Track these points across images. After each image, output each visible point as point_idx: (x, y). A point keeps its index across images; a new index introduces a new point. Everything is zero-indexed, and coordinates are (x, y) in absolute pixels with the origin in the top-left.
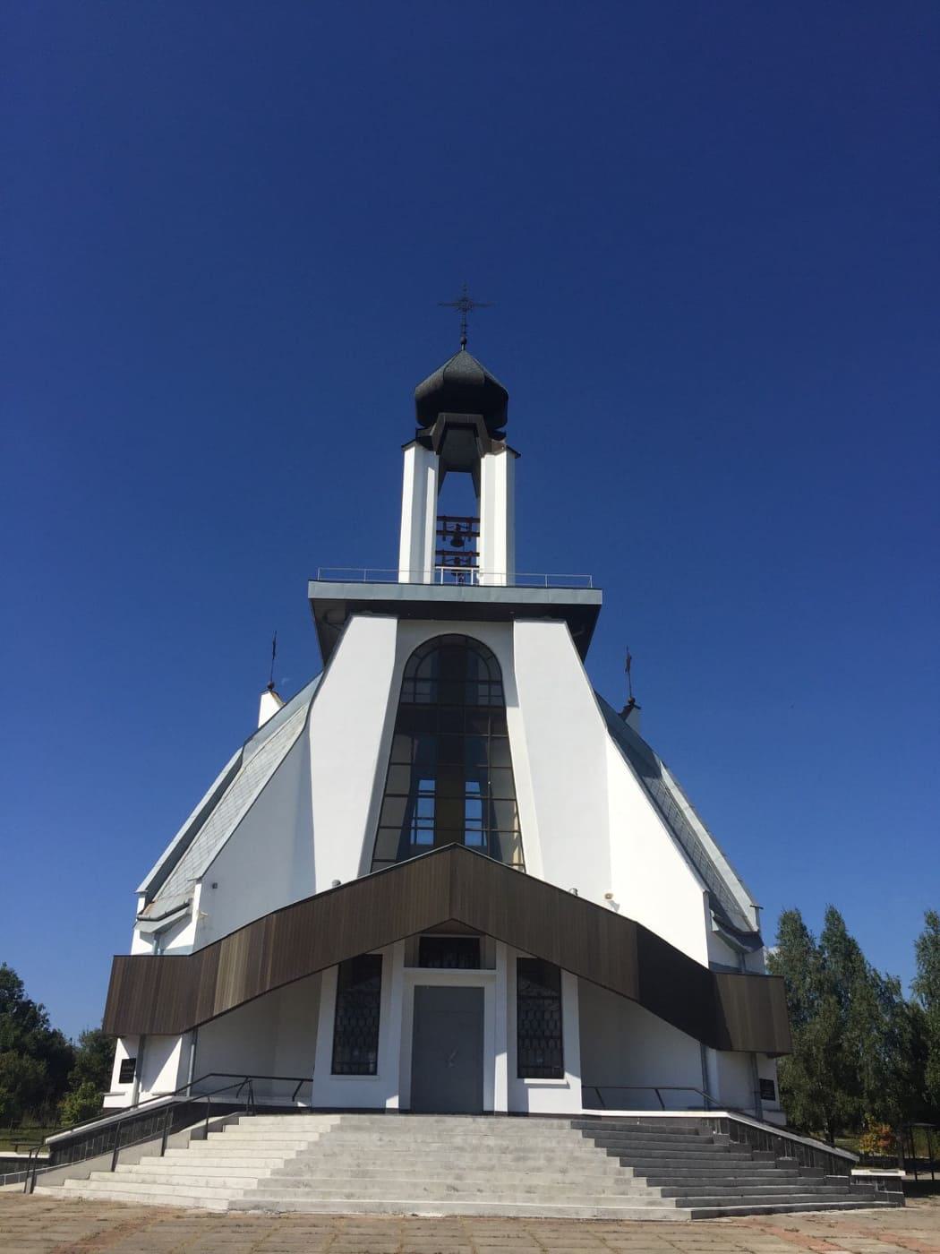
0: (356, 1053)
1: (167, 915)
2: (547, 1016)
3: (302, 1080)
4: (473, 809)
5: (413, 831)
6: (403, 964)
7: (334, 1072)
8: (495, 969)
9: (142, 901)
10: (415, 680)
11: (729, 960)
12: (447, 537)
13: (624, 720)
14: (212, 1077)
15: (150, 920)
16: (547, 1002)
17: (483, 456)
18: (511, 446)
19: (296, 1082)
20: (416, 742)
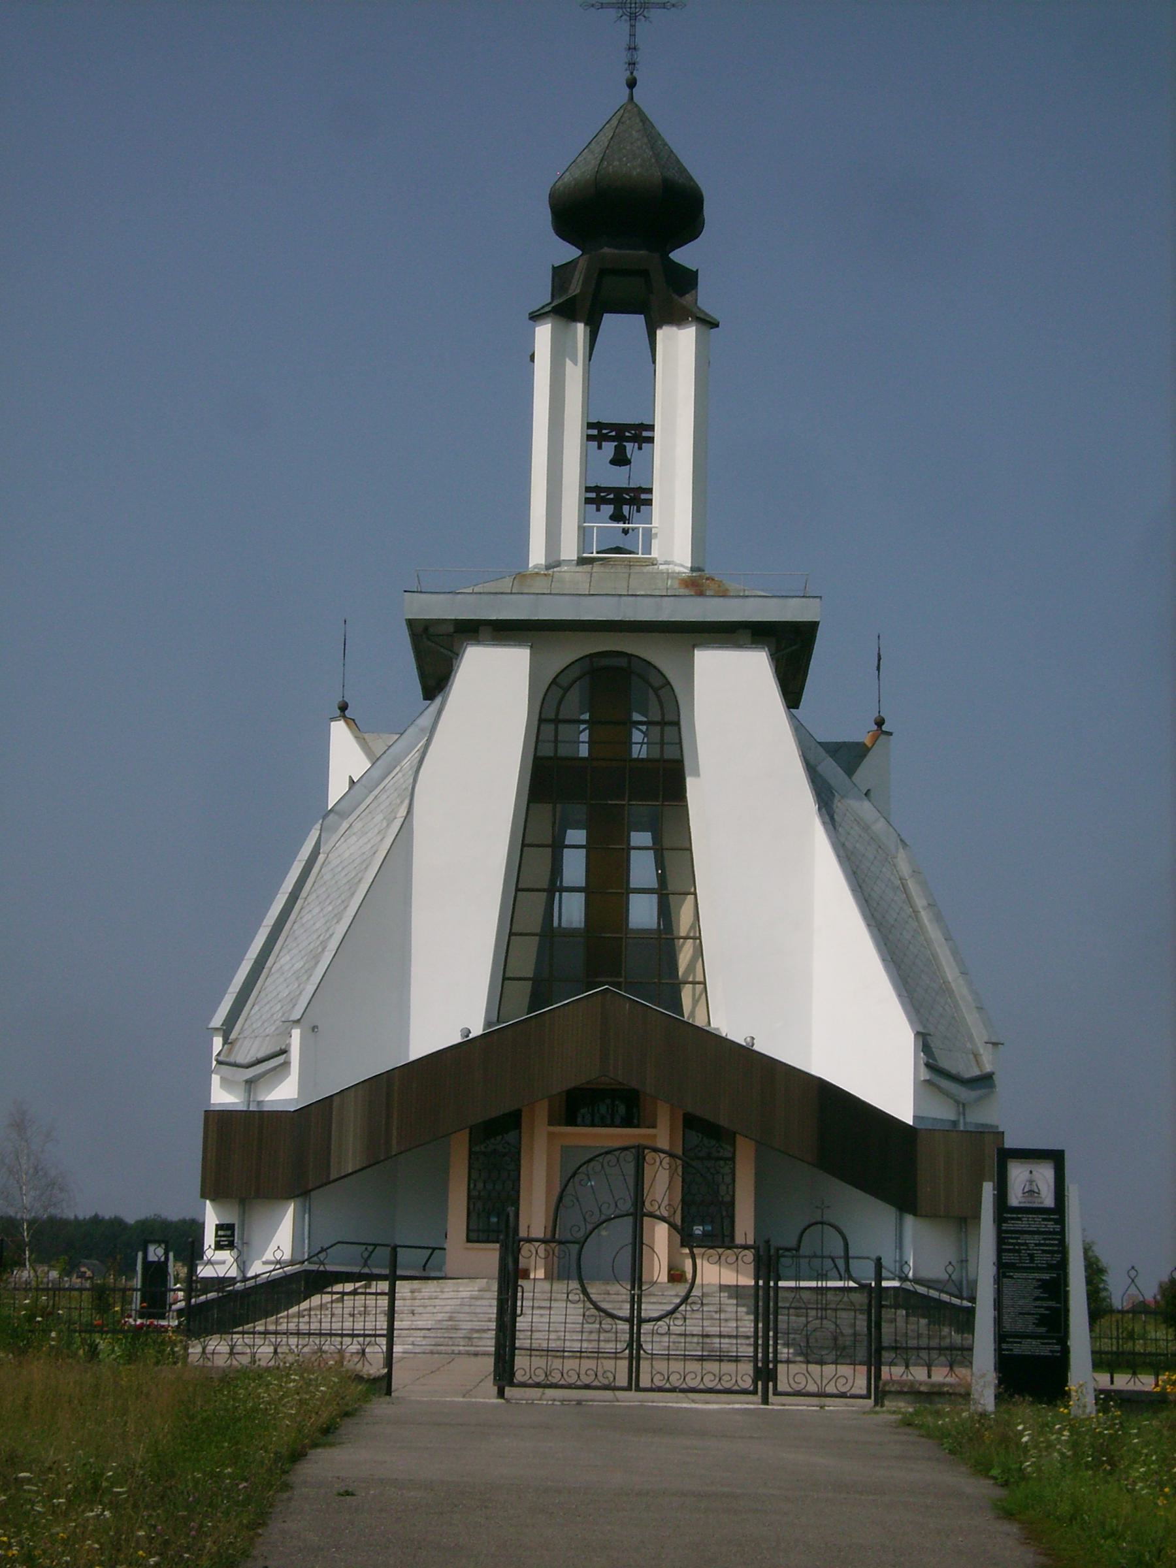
1: (259, 1062)
3: (434, 1249)
4: (642, 868)
5: (557, 894)
7: (469, 1240)
9: (218, 1043)
10: (557, 721)
11: (942, 1111)
12: (602, 507)
14: (842, 1243)
17: (661, 327)
19: (424, 1251)
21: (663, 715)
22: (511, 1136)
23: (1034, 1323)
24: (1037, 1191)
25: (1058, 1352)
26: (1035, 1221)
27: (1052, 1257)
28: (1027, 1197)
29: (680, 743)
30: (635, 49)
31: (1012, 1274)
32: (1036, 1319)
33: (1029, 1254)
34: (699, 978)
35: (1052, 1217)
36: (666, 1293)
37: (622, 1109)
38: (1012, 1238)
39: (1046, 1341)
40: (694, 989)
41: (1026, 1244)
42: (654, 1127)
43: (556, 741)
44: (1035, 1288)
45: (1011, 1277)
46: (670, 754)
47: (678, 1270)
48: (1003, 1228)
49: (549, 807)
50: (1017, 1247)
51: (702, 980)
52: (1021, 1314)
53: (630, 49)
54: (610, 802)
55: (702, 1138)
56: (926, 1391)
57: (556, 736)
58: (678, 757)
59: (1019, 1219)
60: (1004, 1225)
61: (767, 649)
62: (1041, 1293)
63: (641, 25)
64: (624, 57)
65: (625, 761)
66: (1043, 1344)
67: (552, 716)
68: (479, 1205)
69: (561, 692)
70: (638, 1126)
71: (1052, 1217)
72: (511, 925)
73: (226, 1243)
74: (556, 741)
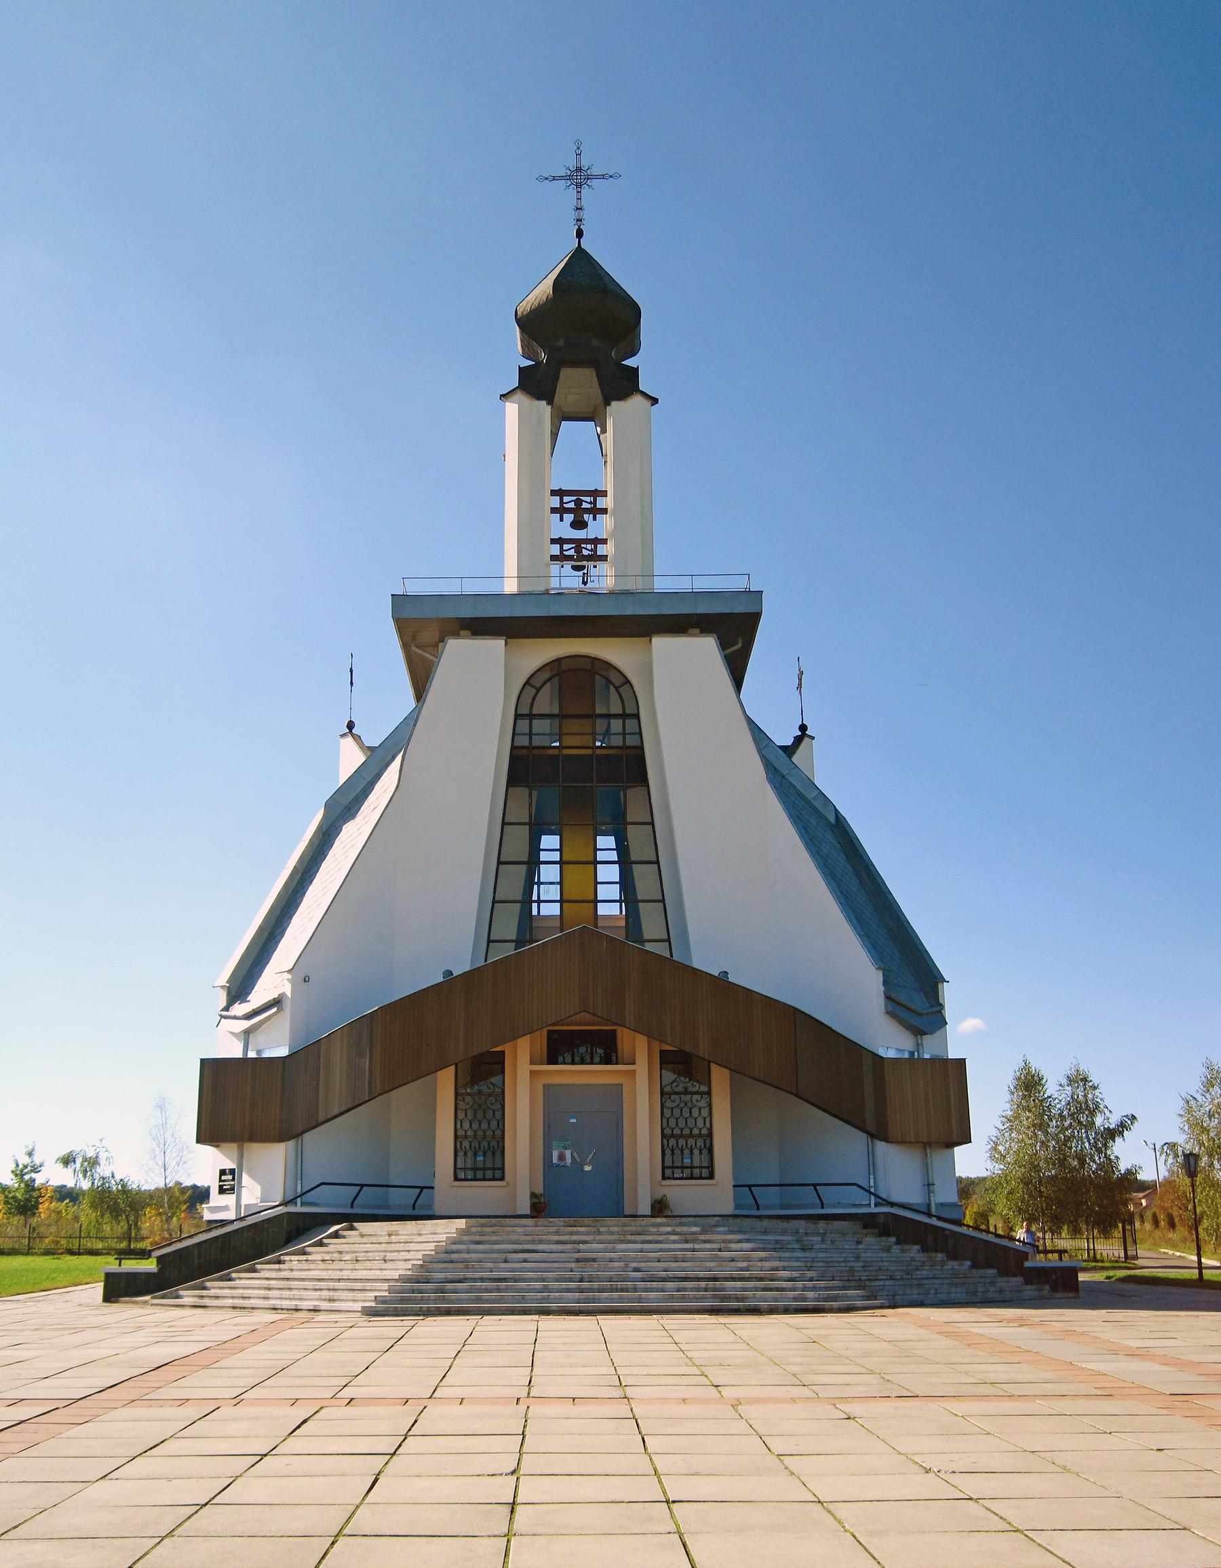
0: (480, 1158)
2: (695, 1112)
3: (422, 1188)
5: (536, 886)
6: (529, 1063)
8: (635, 1064)
10: (531, 716)
13: (790, 756)
15: (235, 1018)
16: (695, 1097)
18: (899, 1048)
20: (535, 793)
22: (496, 1080)
30: (581, 209)
42: (634, 1063)
46: (631, 741)
49: (526, 790)
53: (577, 209)
57: (531, 738)
63: (585, 191)
64: (573, 215)
67: (527, 712)
68: (466, 1144)
69: (535, 691)
70: (617, 1063)
72: (494, 893)
73: (229, 1187)
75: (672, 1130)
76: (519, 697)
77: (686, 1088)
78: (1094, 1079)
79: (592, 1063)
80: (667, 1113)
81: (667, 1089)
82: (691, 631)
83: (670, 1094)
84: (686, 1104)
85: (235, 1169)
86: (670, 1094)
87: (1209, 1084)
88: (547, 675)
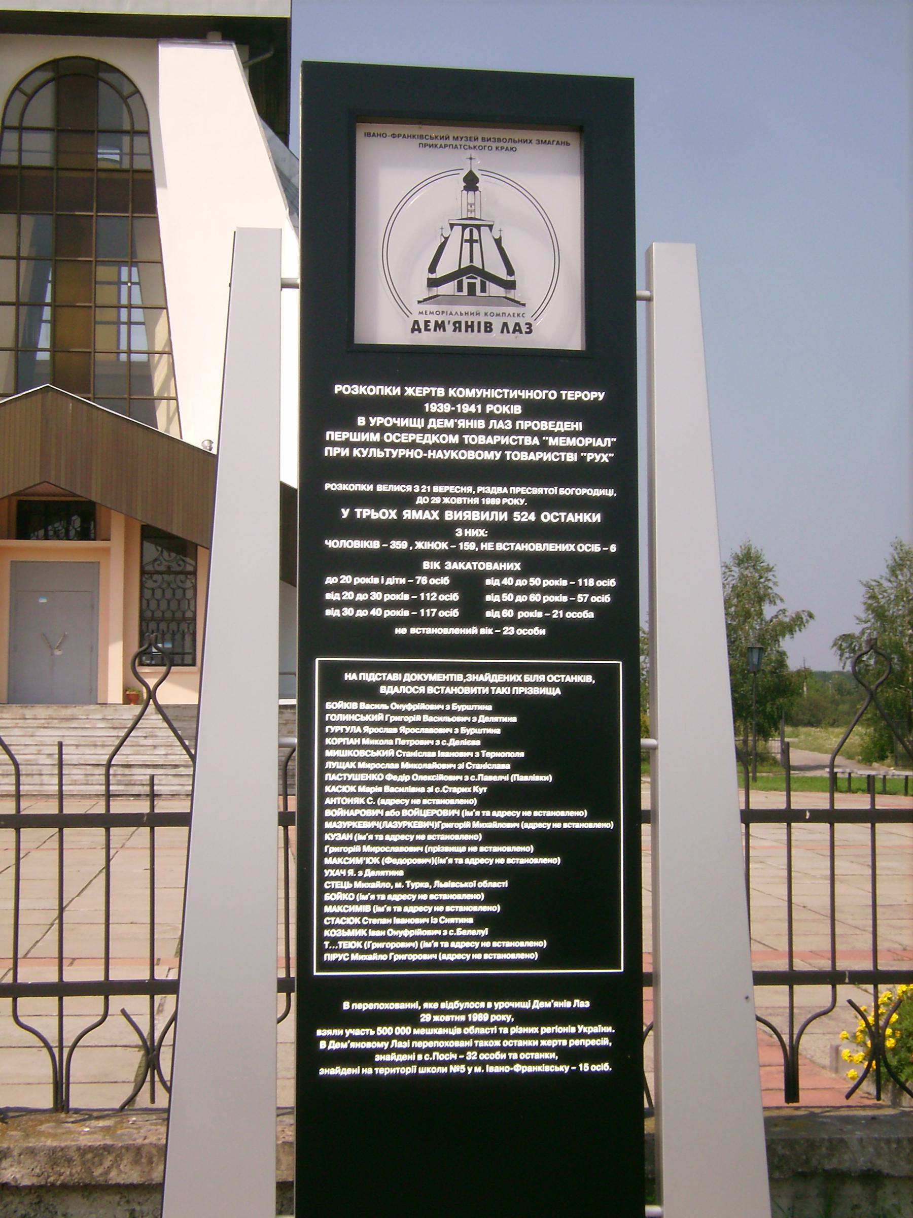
21: (132, 124)
23: (481, 920)
24: (502, 274)
25: (595, 1055)
26: (488, 417)
27: (571, 591)
28: (450, 300)
29: (150, 154)
31: (371, 677)
32: (492, 896)
33: (453, 574)
34: (173, 395)
35: (571, 395)
36: (90, 717)
37: (77, 521)
38: (376, 500)
39: (538, 1005)
40: (168, 405)
41: (442, 530)
43: (20, 150)
44: (489, 743)
45: (369, 692)
46: (140, 164)
47: (134, 691)
48: (331, 452)
50: (399, 545)
51: (174, 396)
52: (414, 873)
54: (77, 213)
55: (162, 552)
56: (26, 1182)
58: (149, 168)
59: (414, 408)
60: (333, 435)
61: (234, 46)
62: (518, 766)
65: (93, 170)
66: (522, 1018)
69: (25, 98)
71: (571, 395)
74: (20, 150)
75: (153, 612)
76: (9, 100)
77: (169, 567)
78: (768, 558)
79: (68, 538)
80: (148, 594)
81: (149, 568)
82: (211, 34)
83: (151, 574)
84: (169, 585)
85: (294, 812)
86: (151, 574)
87: (895, 569)
88: (48, 75)
